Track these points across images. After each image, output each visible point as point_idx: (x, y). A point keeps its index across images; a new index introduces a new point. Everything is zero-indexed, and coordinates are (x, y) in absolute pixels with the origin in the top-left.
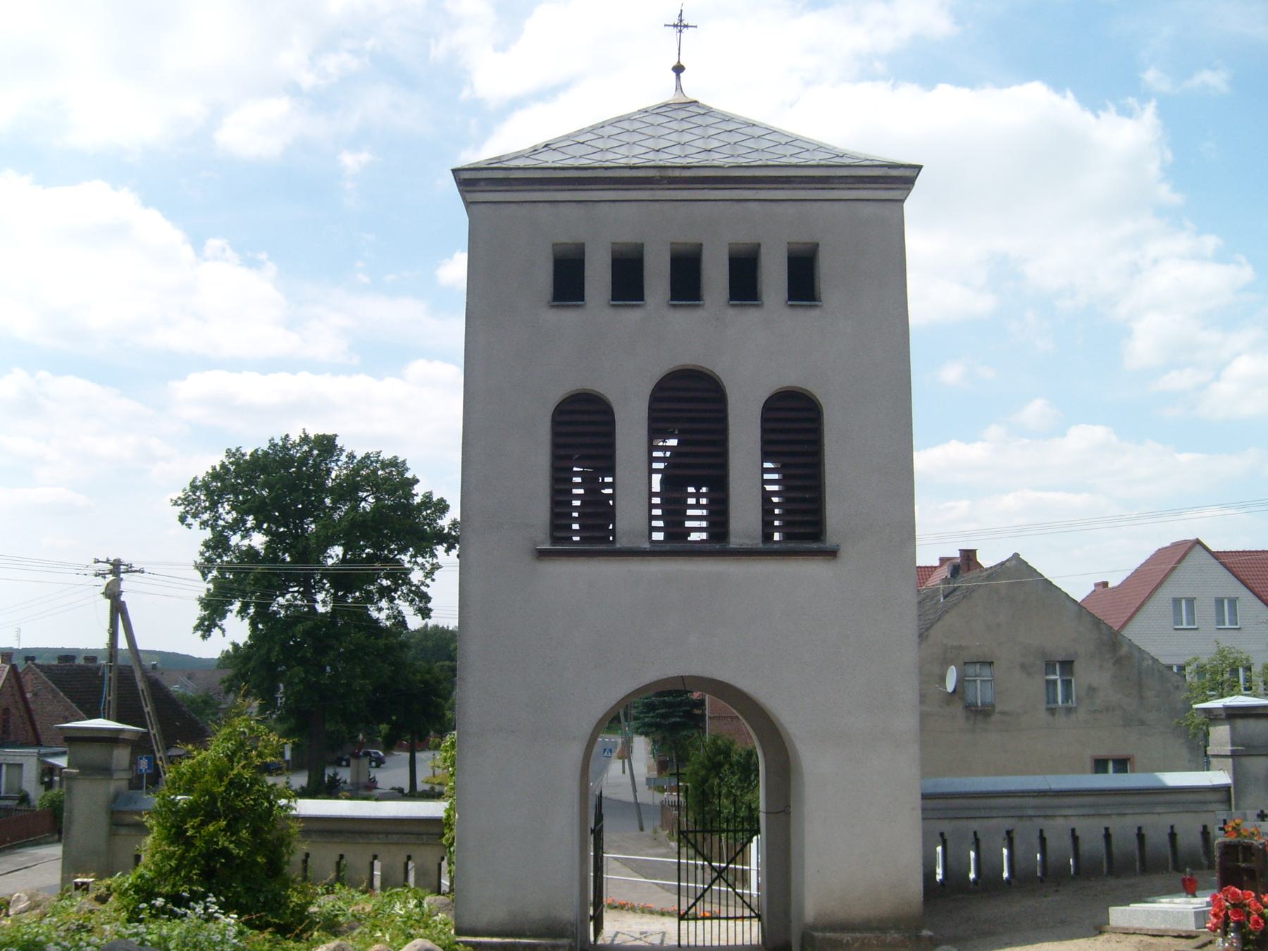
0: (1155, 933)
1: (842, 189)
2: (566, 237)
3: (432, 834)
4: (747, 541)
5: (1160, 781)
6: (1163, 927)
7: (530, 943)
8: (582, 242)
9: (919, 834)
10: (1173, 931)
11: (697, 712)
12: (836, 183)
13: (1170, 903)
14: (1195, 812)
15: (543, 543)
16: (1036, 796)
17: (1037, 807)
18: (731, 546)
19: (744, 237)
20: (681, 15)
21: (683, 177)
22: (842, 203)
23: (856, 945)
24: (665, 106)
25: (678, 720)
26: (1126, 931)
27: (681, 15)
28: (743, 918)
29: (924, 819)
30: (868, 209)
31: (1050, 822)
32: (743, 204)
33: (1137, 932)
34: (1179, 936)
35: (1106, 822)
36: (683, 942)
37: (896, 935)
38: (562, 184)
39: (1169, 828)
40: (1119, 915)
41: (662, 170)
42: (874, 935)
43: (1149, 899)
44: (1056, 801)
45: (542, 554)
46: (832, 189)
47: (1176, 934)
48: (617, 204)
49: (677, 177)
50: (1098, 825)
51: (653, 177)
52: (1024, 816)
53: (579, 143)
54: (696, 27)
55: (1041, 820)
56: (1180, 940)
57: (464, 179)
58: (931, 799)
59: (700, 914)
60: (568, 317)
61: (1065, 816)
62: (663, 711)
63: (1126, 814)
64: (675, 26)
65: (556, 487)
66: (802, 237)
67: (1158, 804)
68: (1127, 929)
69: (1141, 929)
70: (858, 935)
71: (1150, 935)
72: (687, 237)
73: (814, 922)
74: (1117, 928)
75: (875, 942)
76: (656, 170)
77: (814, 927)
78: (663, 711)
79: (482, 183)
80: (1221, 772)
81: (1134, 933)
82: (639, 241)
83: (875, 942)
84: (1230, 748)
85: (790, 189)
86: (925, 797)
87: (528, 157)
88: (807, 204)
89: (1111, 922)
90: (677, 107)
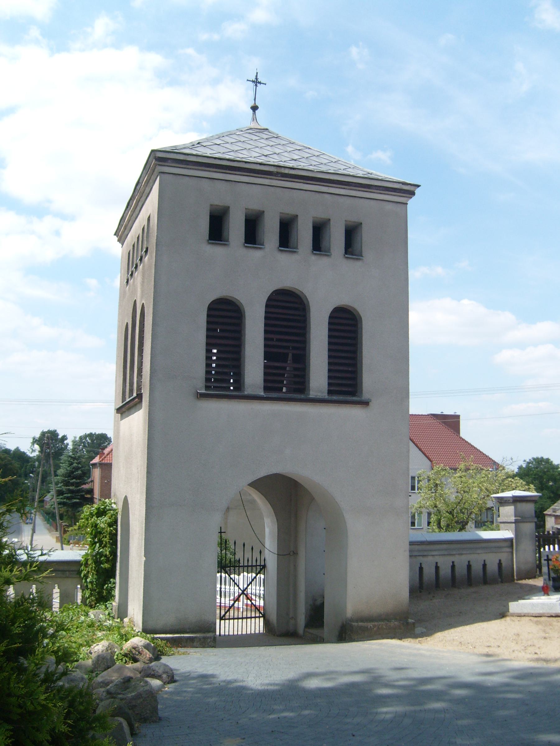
0: (537, 615)
1: (377, 193)
2: (219, 202)
3: (72, 571)
4: (319, 394)
5: (479, 536)
6: (541, 612)
7: (190, 636)
8: (228, 205)
9: (408, 564)
10: (548, 613)
11: (89, 496)
12: (374, 189)
13: (538, 599)
14: (496, 553)
15: (200, 389)
16: (419, 544)
17: (419, 551)
18: (310, 396)
19: (321, 215)
20: (257, 76)
21: (290, 174)
22: (375, 201)
23: (375, 629)
24: (250, 129)
25: (78, 500)
26: (520, 615)
27: (257, 76)
28: (255, 617)
29: (410, 556)
30: (389, 206)
31: (425, 559)
32: (321, 194)
33: (526, 615)
34: (552, 616)
35: (452, 559)
36: (222, 633)
37: (396, 623)
38: (216, 168)
39: (435, 564)
40: (514, 606)
41: (278, 168)
42: (384, 623)
43: (526, 597)
44: (428, 547)
45: (202, 396)
46: (372, 192)
47: (549, 615)
48: (249, 185)
49: (286, 174)
50: (450, 559)
51: (273, 172)
52: (413, 556)
53: (216, 144)
54: (265, 84)
55: (421, 558)
56: (552, 618)
57: (159, 157)
58: (446, 544)
59: (232, 616)
60: (217, 251)
61: (433, 555)
62: (69, 495)
63: (463, 554)
64: (260, 83)
65: (208, 355)
66: (353, 218)
67: (477, 548)
68: (520, 614)
69: (528, 614)
70: (376, 623)
71: (533, 617)
72: (290, 211)
73: (351, 617)
74: (514, 614)
75: (385, 627)
76: (275, 167)
77: (352, 620)
78: (69, 495)
79: (169, 161)
80: (507, 531)
81: (524, 616)
82: (261, 209)
83: (385, 627)
84: (514, 518)
85: (349, 189)
86: (412, 543)
87: (191, 149)
88: (356, 199)
89: (510, 611)
90: (258, 131)
